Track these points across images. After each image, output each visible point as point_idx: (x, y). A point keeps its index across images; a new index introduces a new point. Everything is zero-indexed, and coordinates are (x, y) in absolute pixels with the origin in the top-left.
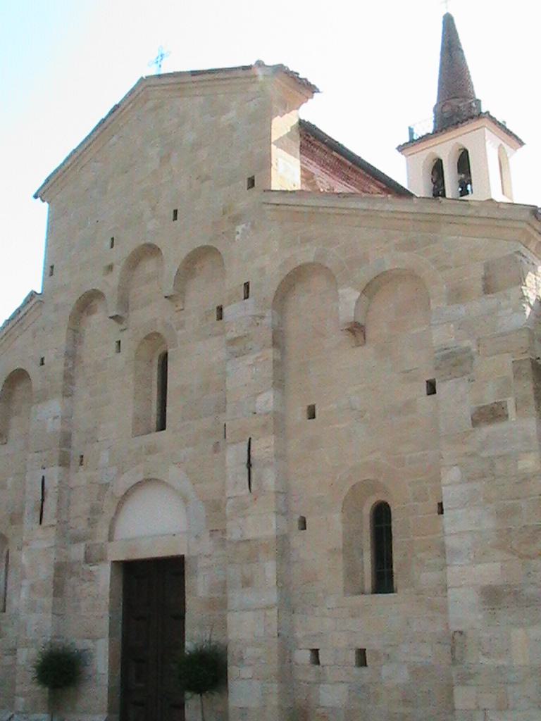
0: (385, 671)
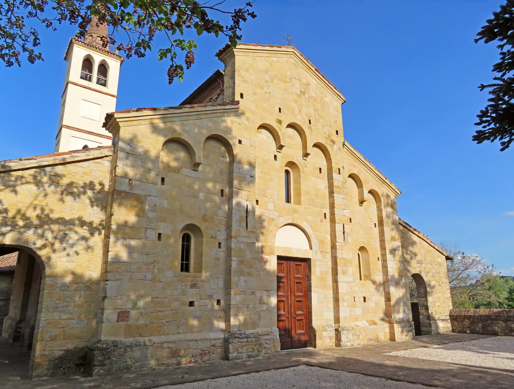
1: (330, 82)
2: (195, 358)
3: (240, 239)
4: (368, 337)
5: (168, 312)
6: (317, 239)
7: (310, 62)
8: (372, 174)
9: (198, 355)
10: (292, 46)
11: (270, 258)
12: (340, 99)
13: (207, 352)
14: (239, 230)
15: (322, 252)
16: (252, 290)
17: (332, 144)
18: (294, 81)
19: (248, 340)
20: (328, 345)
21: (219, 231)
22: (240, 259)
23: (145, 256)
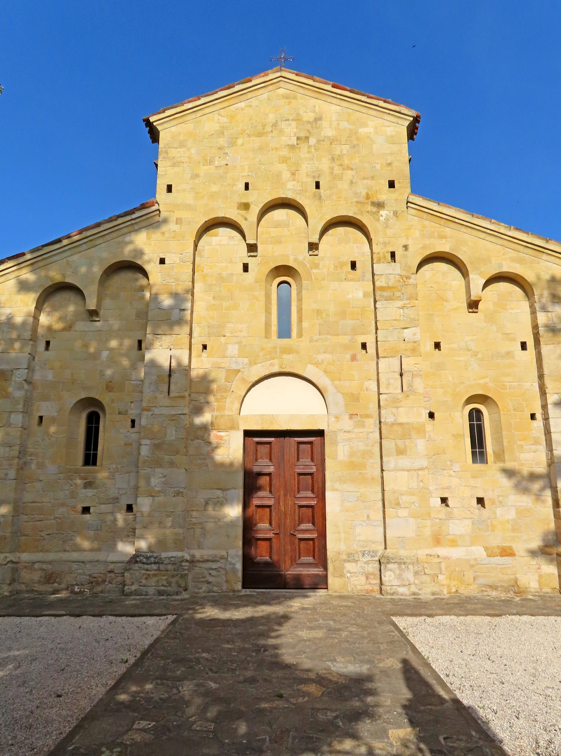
0: (499, 511)
1: (371, 95)
2: (82, 586)
3: (157, 411)
4: (481, 581)
5: (50, 521)
6: (341, 393)
7: (317, 78)
8: (500, 241)
9: (86, 583)
10: (275, 69)
11: (228, 435)
12: (402, 118)
13: (100, 579)
14: (156, 398)
15: (351, 416)
16: (176, 489)
17: (374, 209)
18: (283, 125)
19: (159, 567)
20: (359, 587)
21: (132, 402)
22: (157, 442)
23: (8, 449)
